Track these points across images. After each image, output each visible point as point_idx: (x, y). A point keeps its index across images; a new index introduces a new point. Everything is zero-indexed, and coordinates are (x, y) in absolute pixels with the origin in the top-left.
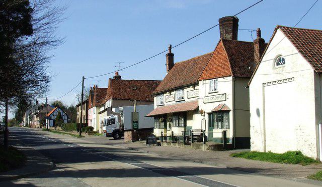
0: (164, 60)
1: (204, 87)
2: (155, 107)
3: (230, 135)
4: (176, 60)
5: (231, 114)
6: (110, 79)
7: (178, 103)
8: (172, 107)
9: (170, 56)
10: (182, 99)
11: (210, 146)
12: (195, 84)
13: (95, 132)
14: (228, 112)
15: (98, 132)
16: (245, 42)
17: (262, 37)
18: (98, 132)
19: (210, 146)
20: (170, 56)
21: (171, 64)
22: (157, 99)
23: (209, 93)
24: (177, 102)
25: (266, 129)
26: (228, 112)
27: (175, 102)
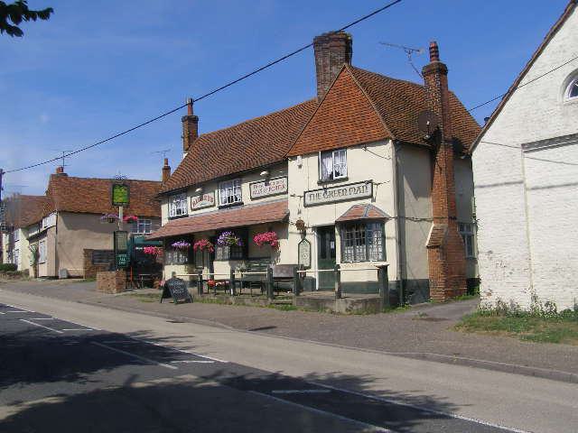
0: (179, 128)
1: (303, 173)
2: (165, 221)
3: (393, 275)
4: (203, 129)
5: (390, 229)
6: (53, 176)
7: (226, 210)
8: (210, 218)
9: (192, 121)
10: (234, 203)
11: (353, 303)
12: (278, 167)
13: (20, 274)
14: (382, 221)
15: (27, 273)
16: (285, 112)
17: (443, 59)
18: (27, 273)
19: (353, 303)
20: (192, 121)
21: (191, 138)
22: (167, 211)
23: (252, 199)
24: (220, 208)
25: (409, 258)
26: (382, 221)
27: (216, 208)
